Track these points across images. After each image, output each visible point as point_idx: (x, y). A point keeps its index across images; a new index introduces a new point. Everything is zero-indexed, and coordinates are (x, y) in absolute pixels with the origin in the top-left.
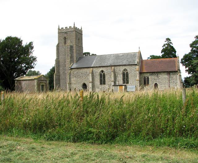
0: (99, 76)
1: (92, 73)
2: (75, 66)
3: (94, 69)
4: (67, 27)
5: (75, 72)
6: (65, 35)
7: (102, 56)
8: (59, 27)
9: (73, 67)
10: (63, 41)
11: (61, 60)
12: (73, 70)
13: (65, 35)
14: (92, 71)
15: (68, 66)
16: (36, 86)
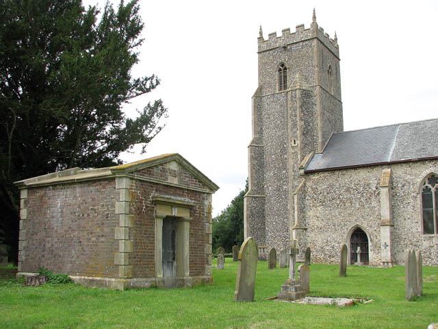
0: (419, 198)
1: (392, 187)
2: (319, 162)
3: (399, 171)
4: (289, 30)
5: (322, 187)
6: (284, 57)
7: (417, 123)
8: (261, 33)
9: (312, 167)
10: (277, 77)
11: (269, 146)
12: (315, 177)
13: (284, 57)
14: (391, 177)
15: (295, 162)
16: (124, 221)
